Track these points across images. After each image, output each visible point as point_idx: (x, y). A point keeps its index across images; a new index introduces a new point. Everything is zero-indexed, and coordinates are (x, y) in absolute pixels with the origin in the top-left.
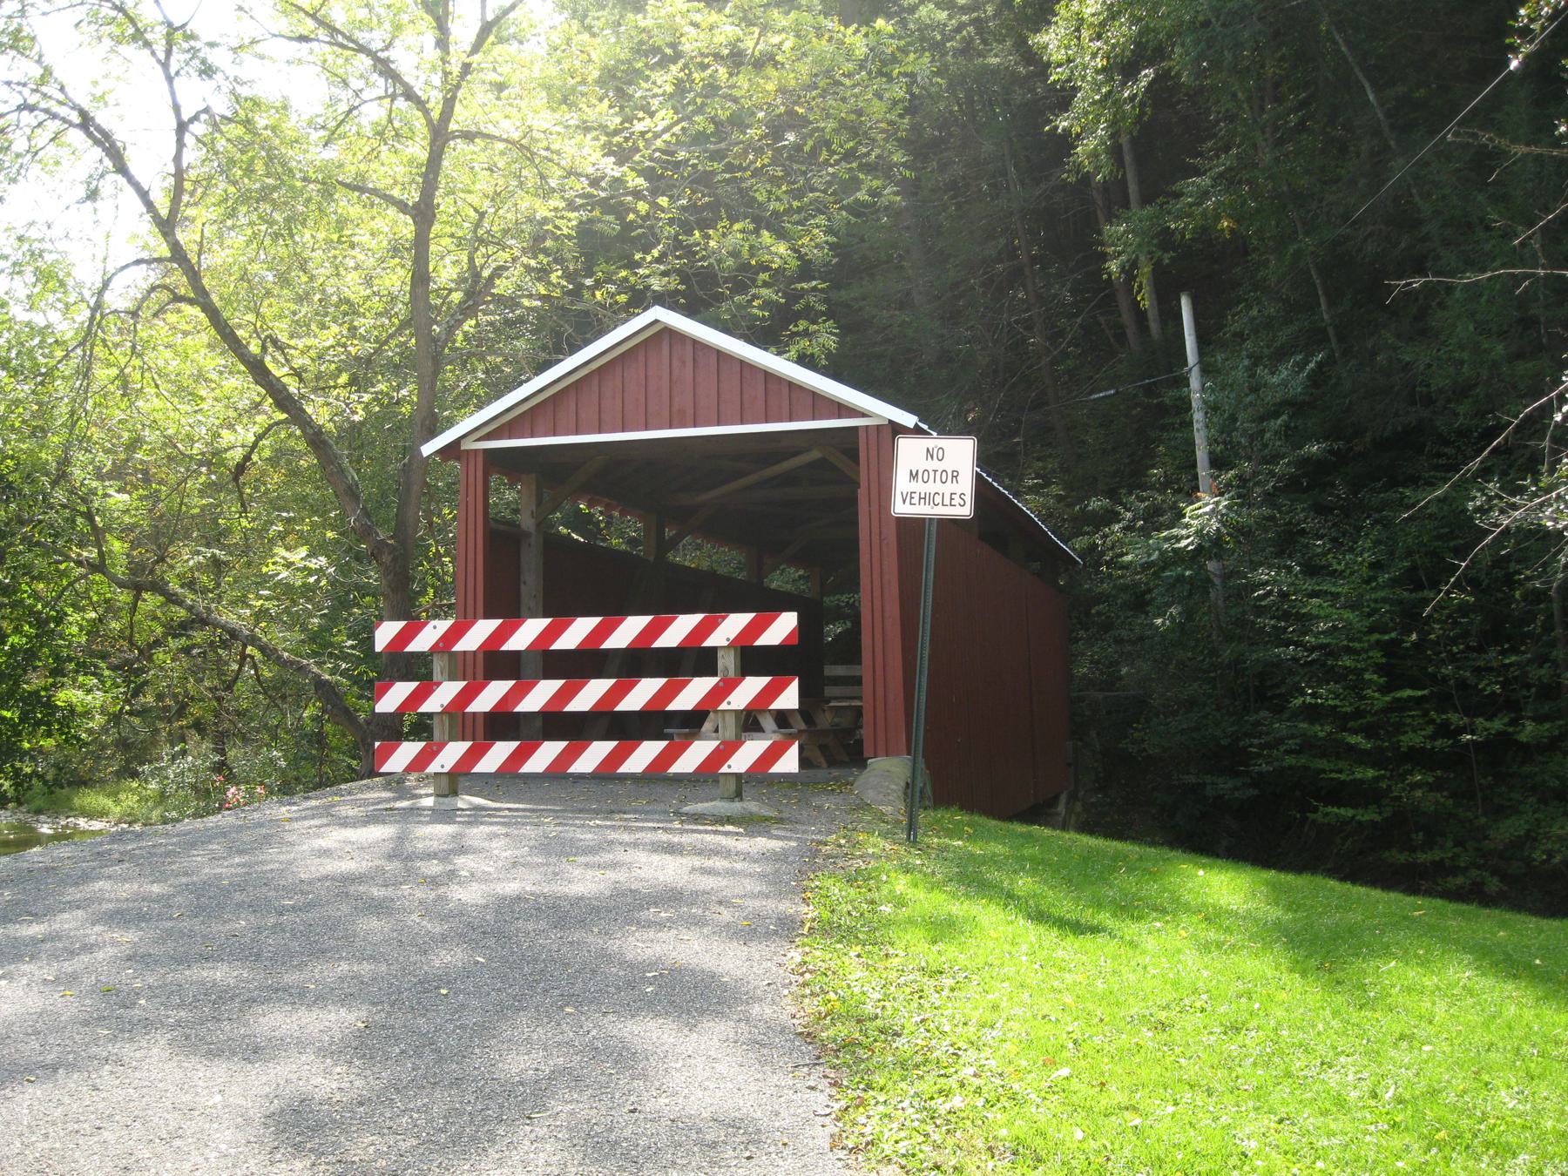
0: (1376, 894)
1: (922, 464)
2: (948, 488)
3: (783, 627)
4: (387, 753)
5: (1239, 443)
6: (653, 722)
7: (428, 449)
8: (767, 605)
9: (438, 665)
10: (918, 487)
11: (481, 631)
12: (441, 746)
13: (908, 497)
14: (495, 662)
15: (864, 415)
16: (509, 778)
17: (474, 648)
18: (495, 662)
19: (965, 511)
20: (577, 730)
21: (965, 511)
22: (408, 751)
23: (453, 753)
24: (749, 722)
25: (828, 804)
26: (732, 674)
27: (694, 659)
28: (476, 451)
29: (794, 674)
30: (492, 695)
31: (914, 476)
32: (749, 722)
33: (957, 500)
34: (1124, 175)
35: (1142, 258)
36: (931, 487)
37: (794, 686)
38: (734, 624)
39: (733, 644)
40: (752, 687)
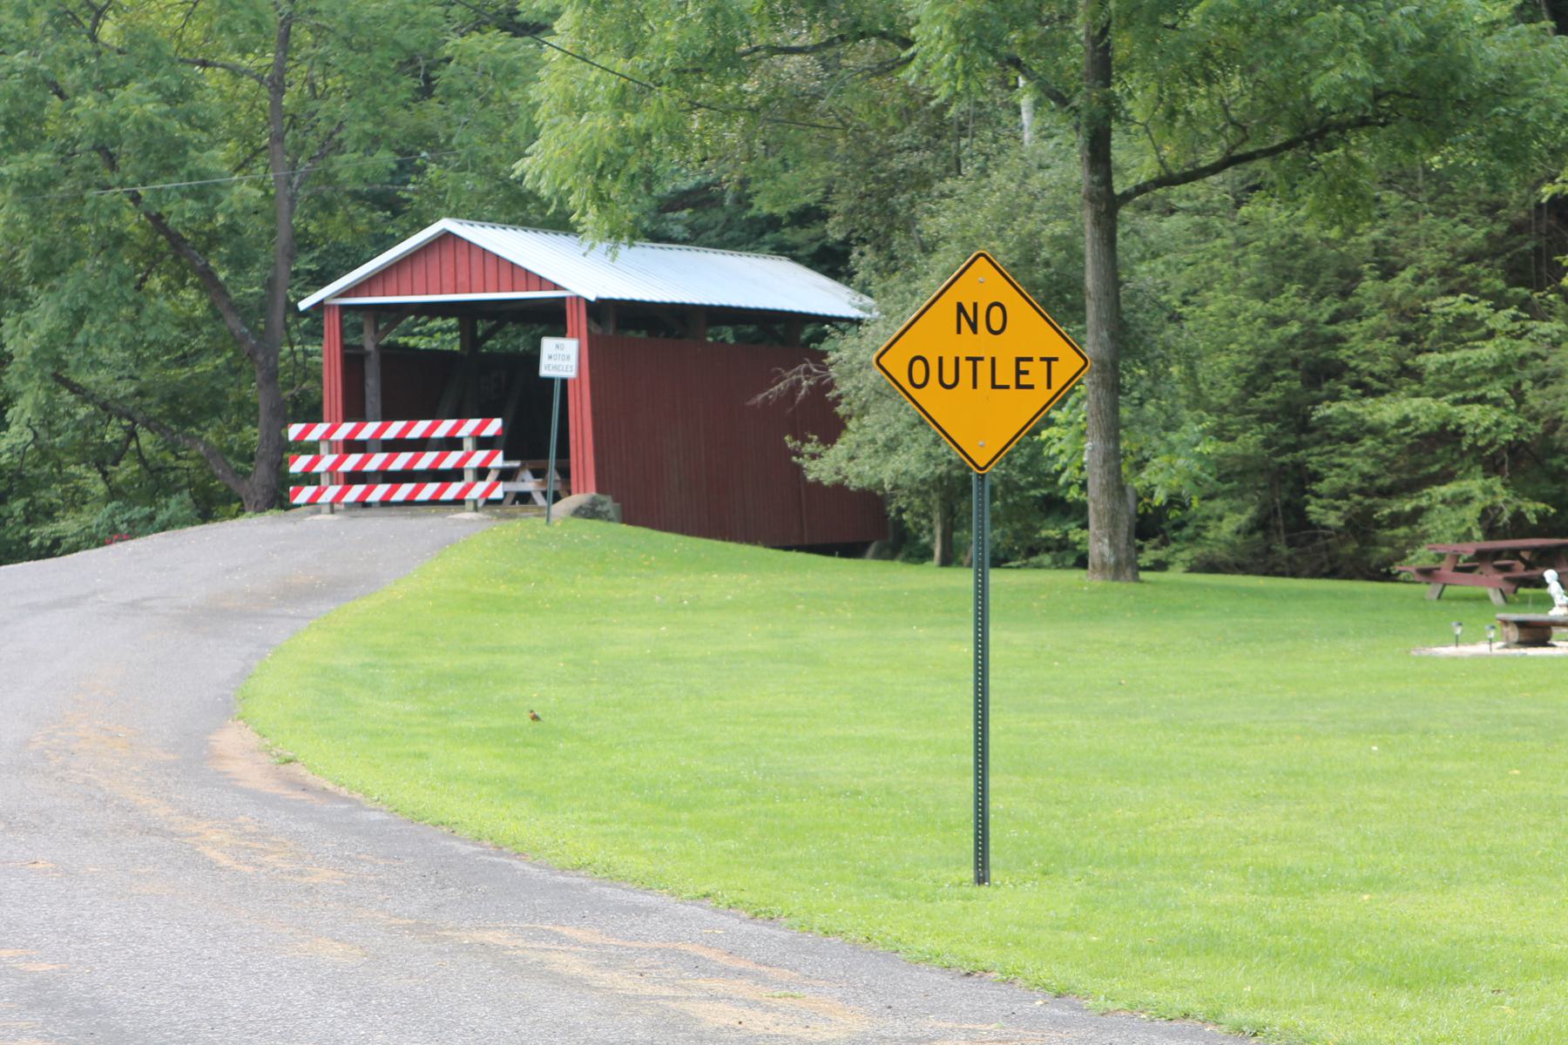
1: (554, 352)
2: (566, 363)
3: (494, 427)
4: (296, 493)
6: (434, 475)
9: (323, 447)
10: (552, 362)
11: (345, 429)
13: (547, 367)
14: (351, 446)
15: (542, 283)
18: (351, 446)
19: (544, 372)
21: (544, 372)
22: (307, 492)
24: (482, 473)
25: (1105, 334)
27: (452, 443)
30: (352, 461)
32: (482, 473)
34: (1526, 549)
35: (1360, 450)
36: (558, 363)
37: (500, 455)
38: (471, 425)
40: (481, 455)
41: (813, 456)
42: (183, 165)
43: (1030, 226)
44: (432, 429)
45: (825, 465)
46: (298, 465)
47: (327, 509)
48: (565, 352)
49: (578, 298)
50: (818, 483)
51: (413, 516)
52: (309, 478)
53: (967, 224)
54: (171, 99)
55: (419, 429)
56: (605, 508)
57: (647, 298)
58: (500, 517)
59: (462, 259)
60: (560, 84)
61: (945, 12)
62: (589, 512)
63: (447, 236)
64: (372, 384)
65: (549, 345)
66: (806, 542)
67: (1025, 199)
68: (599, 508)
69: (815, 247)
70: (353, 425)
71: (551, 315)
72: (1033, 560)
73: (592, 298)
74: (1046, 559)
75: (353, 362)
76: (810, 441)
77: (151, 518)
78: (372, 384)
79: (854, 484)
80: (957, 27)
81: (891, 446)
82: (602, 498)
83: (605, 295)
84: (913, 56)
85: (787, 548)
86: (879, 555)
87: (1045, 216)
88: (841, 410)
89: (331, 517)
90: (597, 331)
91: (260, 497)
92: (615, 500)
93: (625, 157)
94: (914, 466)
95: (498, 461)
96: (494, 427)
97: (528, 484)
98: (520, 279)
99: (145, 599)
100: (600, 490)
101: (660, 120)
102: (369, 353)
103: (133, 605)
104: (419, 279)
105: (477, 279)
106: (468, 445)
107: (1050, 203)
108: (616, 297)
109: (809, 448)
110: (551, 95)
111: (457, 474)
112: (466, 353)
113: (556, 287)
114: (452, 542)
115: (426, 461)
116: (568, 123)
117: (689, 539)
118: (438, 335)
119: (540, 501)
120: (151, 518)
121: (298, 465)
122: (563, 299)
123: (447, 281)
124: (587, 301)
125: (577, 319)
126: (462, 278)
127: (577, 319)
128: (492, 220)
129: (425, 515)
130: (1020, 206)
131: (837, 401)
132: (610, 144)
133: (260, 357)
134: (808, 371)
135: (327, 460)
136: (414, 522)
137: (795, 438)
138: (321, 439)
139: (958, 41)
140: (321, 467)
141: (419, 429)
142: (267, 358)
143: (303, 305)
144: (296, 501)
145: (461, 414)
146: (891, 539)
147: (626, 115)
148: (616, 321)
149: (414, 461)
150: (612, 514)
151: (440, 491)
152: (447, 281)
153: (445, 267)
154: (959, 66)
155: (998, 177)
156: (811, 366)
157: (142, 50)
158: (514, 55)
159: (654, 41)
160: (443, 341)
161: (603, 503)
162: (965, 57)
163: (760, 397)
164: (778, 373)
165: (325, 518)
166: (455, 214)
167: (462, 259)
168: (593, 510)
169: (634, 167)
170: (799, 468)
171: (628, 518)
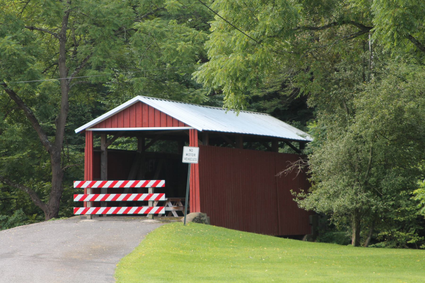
0: (237, 232)
1: (188, 152)
2: (193, 157)
3: (162, 183)
4: (76, 210)
5: (6, 152)
6: (135, 203)
7: (77, 131)
8: (159, 179)
10: (188, 157)
12: (89, 208)
15: (179, 123)
16: (93, 215)
17: (87, 181)
19: (184, 161)
20: (119, 204)
21: (184, 161)
23: (92, 209)
26: (151, 193)
27: (144, 190)
28: (90, 131)
29: (164, 193)
31: (187, 155)
33: (195, 160)
37: (164, 195)
38: (152, 182)
39: (152, 187)
40: (156, 195)
41: (301, 199)
42: (25, 69)
43: (400, 103)
44: (124, 184)
45: (307, 203)
46: (78, 198)
47: (89, 217)
48: (193, 153)
49: (194, 130)
50: (300, 208)
51: (126, 221)
52: (81, 204)
53: (373, 102)
54: (25, 42)
55: (119, 184)
56: (204, 219)
57: (222, 130)
58: (163, 222)
59: (145, 113)
60: (219, 41)
61: (390, 13)
62: (198, 220)
63: (139, 103)
64: (104, 165)
65: (186, 150)
66: (280, 235)
67: (397, 92)
68: (202, 219)
69: (273, 109)
70: (112, 182)
71: (183, 137)
72: (378, 244)
73: (201, 130)
74: (383, 244)
75: (97, 154)
76: (301, 192)
77: (6, 220)
78: (104, 165)
79: (318, 210)
80: (395, 19)
81: (336, 195)
82: (203, 214)
83: (206, 129)
84: (374, 31)
85: (285, 237)
86: (308, 240)
87: (406, 100)
88: (312, 178)
89: (91, 220)
90: (201, 144)
91: (52, 212)
92: (208, 215)
93: (247, 73)
94: (347, 203)
95: (163, 198)
96: (162, 183)
97: (171, 208)
98: (169, 121)
99: (39, 254)
100: (201, 211)
101: (263, 57)
102: (103, 152)
103: (35, 256)
104: (126, 121)
105: (151, 121)
106: (150, 191)
107: (407, 94)
108: (210, 129)
109: (300, 195)
110: (214, 46)
111: (145, 203)
112: (140, 152)
113: (185, 125)
114: (149, 232)
115: (122, 197)
116: (223, 58)
117: (244, 232)
118: (120, 145)
119: (176, 215)
120: (6, 220)
121: (78, 198)
122: (188, 130)
123: (139, 121)
124: (198, 131)
125: (193, 138)
126: (145, 120)
127: (193, 138)
128: (162, 98)
129: (131, 220)
130: (394, 95)
131: (309, 176)
132: (243, 67)
133: (53, 152)
134: (301, 163)
135: (90, 196)
136: (128, 223)
137: (294, 191)
138: (87, 187)
139: (395, 25)
140: (88, 199)
141: (119, 184)
142: (56, 153)
143: (77, 131)
144: (76, 213)
145: (148, 178)
146: (312, 234)
147: (248, 55)
148: (210, 140)
149: (116, 197)
150: (207, 221)
151: (128, 210)
152: (139, 121)
153: (137, 116)
154: (395, 36)
155: (384, 82)
156: (302, 160)
157: (10, 23)
158: (164, 29)
159: (261, 24)
160: (122, 147)
161: (203, 216)
162: (398, 32)
163: (281, 173)
164: (289, 163)
165: (88, 221)
166: (144, 94)
167: (145, 113)
168: (200, 219)
169: (252, 76)
170: (296, 203)
171: (212, 223)
